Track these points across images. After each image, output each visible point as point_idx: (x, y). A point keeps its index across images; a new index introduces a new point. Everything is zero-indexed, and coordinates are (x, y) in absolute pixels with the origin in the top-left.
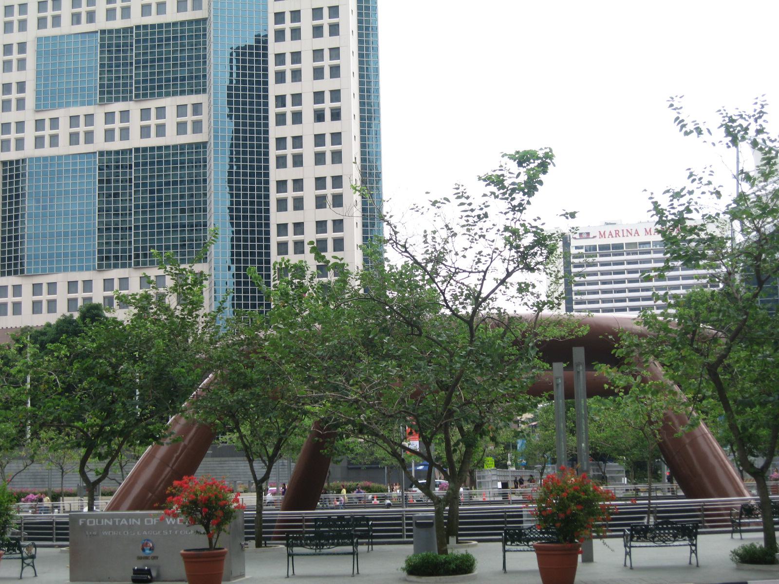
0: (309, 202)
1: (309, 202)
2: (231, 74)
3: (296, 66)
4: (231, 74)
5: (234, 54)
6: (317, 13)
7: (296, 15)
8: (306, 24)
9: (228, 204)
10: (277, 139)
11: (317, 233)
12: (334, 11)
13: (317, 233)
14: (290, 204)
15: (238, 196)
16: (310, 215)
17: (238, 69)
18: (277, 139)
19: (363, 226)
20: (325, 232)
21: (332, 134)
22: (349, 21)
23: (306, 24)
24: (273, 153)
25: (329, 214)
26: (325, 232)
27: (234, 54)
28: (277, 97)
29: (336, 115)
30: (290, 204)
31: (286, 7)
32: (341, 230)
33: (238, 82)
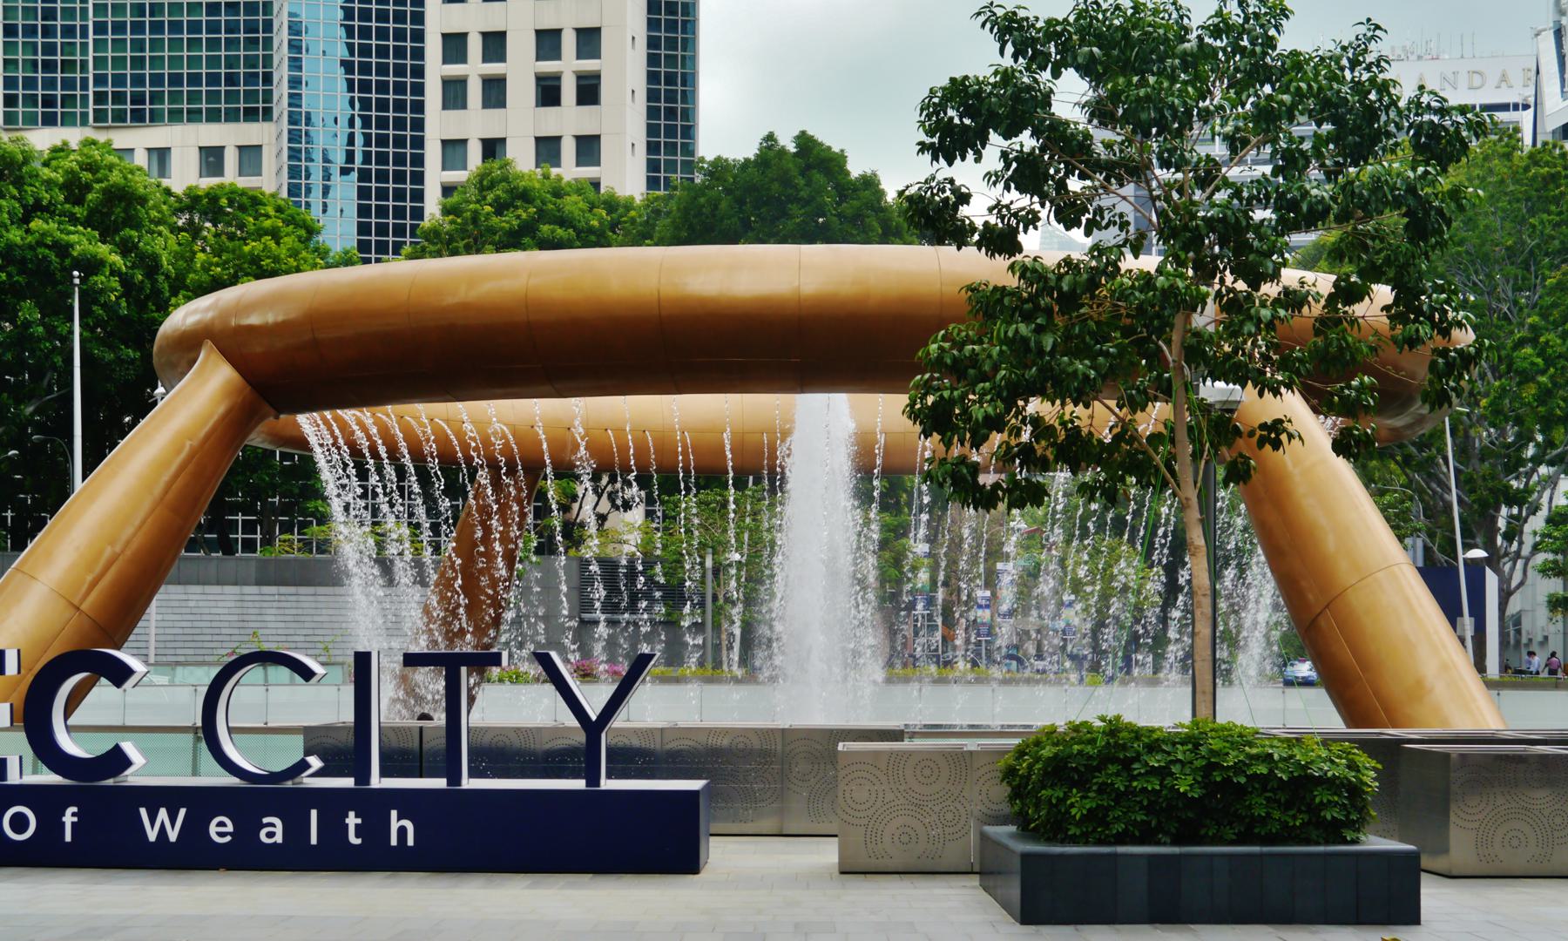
0: (521, 90)
1: (521, 90)
2: (351, 140)
3: (494, 68)
4: (351, 140)
5: (358, 122)
6: (548, 42)
7: (495, 44)
8: (521, 68)
9: (341, 52)
10: (445, 143)
11: (538, 59)
12: (589, 40)
13: (538, 59)
14: (475, 92)
15: (366, 32)
16: (521, 123)
17: (367, 143)
18: (445, 143)
19: (650, 46)
20: (558, 57)
21: (579, 31)
22: (625, 67)
23: (521, 68)
24: (435, 69)
25: (568, 120)
26: (558, 57)
27: (358, 122)
28: (446, 37)
29: (589, 91)
30: (475, 92)
31: (472, 20)
32: (596, 54)
33: (367, 157)
